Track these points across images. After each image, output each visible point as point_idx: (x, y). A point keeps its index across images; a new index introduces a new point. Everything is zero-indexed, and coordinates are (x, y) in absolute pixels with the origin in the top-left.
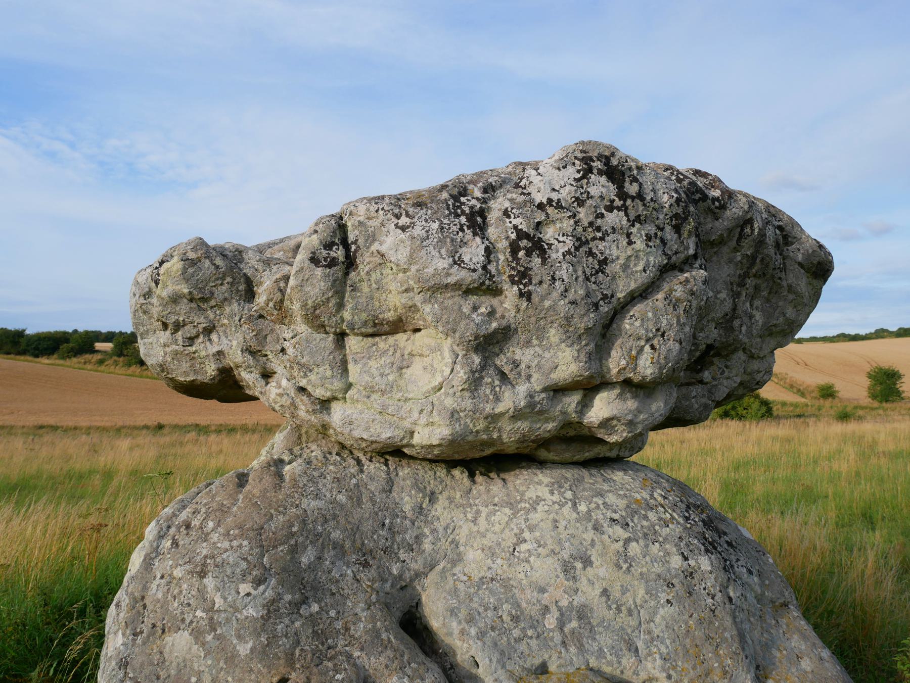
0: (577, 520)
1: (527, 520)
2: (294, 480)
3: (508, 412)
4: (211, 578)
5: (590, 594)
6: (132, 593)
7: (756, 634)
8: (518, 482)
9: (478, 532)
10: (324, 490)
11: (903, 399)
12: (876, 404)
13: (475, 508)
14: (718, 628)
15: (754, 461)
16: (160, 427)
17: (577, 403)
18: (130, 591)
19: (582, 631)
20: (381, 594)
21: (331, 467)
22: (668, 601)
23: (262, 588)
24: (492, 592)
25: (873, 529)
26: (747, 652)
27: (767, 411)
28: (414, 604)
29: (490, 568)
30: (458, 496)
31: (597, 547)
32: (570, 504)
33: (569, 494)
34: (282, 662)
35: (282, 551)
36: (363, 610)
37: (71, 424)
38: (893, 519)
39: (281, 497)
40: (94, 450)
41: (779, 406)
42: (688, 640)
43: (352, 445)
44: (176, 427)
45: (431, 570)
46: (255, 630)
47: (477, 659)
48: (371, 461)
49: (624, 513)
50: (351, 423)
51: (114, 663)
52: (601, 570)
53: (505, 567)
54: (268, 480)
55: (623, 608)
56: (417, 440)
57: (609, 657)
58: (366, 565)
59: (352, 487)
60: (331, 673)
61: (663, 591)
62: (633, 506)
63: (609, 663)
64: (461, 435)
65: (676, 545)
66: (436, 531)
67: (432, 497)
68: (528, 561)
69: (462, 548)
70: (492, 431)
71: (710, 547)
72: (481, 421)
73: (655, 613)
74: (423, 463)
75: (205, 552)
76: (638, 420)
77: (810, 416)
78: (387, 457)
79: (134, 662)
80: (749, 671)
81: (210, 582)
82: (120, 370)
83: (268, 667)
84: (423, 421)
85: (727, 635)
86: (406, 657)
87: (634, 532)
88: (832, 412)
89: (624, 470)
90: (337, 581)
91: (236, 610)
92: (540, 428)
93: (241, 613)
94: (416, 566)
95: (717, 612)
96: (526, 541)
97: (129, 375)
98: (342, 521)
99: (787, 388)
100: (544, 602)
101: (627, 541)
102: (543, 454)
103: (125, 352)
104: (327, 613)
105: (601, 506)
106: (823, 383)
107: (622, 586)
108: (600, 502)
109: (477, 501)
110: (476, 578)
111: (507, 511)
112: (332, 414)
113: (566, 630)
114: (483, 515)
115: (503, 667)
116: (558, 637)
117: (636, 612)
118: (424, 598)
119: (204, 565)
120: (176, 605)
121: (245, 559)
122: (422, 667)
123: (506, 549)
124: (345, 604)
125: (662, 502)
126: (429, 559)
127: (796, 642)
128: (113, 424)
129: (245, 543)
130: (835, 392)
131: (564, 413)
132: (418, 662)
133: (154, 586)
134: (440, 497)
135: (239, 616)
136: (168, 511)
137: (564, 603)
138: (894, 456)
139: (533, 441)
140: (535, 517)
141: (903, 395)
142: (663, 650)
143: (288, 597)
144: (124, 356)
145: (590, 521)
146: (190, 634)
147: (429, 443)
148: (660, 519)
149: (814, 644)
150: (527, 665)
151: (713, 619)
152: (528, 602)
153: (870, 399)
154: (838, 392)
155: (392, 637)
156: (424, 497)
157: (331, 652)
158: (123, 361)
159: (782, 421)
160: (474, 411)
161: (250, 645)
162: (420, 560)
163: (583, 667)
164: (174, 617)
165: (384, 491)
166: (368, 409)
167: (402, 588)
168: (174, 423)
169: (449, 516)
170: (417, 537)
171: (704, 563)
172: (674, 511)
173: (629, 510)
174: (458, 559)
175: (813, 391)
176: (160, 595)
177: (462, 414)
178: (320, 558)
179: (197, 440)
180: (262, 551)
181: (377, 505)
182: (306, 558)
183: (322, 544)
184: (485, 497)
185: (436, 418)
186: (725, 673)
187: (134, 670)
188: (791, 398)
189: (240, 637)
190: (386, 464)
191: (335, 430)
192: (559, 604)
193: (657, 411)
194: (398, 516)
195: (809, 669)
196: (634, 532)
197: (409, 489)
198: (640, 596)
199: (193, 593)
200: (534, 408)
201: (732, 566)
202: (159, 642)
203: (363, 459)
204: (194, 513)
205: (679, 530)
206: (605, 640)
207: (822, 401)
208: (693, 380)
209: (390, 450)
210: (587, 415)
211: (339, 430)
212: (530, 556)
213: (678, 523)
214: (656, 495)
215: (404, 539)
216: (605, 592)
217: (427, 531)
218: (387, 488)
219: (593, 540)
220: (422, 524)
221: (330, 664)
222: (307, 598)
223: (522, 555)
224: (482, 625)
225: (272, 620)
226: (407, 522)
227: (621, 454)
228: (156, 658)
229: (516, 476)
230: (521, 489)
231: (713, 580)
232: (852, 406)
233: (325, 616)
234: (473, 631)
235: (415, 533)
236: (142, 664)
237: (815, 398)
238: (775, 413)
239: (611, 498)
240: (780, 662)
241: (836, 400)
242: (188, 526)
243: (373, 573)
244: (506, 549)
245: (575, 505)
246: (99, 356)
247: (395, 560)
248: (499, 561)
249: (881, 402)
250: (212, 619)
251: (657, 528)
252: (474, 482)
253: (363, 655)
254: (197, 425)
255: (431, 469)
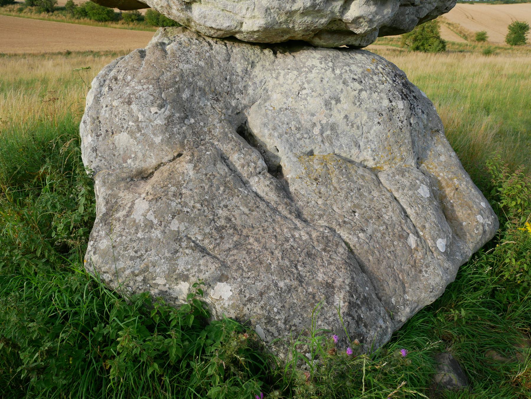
0: (334, 78)
1: (306, 77)
2: (174, 54)
3: (299, 10)
4: (134, 105)
5: (338, 117)
6: (91, 116)
7: (421, 143)
8: (302, 57)
9: (279, 84)
10: (191, 59)
11: (525, 43)
12: (509, 46)
13: (277, 71)
14: (402, 137)
15: (430, 76)
16: (69, 53)
17: (341, 6)
18: (90, 114)
19: (332, 136)
20: (227, 116)
21: (194, 46)
22: (379, 123)
23: (163, 110)
24: (285, 115)
25: (488, 115)
26: (415, 150)
27: (442, 47)
28: (244, 122)
29: (285, 103)
30: (267, 64)
31: (344, 93)
32: (331, 69)
33: (330, 64)
34: (178, 146)
35: (172, 91)
36: (218, 123)
37: (12, 52)
38: (500, 110)
39: (167, 62)
40: (31, 67)
41: (450, 45)
42: (386, 143)
43: (206, 33)
44: (79, 53)
45: (253, 104)
46: (162, 131)
47: (278, 148)
48: (216, 43)
49: (360, 76)
50: (205, 17)
51: (89, 150)
52: (345, 105)
53: (293, 102)
54: (158, 53)
55: (355, 125)
56: (244, 28)
57: (345, 149)
58: (217, 100)
59: (207, 57)
60: (204, 151)
61: (377, 117)
62: (366, 72)
63: (345, 152)
64: (271, 24)
65: (386, 94)
66: (255, 83)
67: (253, 65)
68: (306, 99)
69: (269, 93)
70: (289, 23)
71: (404, 97)
72: (283, 16)
73: (371, 129)
74: (247, 45)
75: (128, 92)
76: (375, 19)
77: (468, 52)
78: (226, 41)
79: (100, 149)
80: (414, 159)
81: (134, 107)
82: (35, 16)
83: (171, 148)
84: (248, 15)
85: (406, 141)
86: (242, 145)
87: (365, 86)
88: (481, 50)
89: (362, 54)
90: (203, 108)
91: (151, 121)
92: (317, 22)
93: (153, 122)
94: (245, 102)
95: (403, 130)
96: (305, 89)
97: (41, 19)
98: (203, 76)
99: (457, 33)
100: (313, 121)
101: (361, 91)
102: (317, 41)
103: (35, 3)
104: (199, 123)
105: (348, 71)
106: (480, 31)
107: (355, 114)
108: (348, 69)
109: (278, 67)
110: (277, 108)
111: (295, 72)
112: (193, 12)
113: (324, 135)
114: (282, 75)
115: (291, 151)
116: (320, 139)
117: (361, 128)
118: (249, 119)
119: (129, 98)
120: (117, 120)
121: (152, 95)
122: (250, 150)
123: (294, 93)
124: (208, 120)
125: (382, 71)
126: (252, 98)
127: (440, 148)
128: (39, 52)
129: (151, 86)
130: (486, 37)
131: (332, 12)
132: (247, 148)
133: (103, 111)
134: (257, 65)
135: (153, 124)
136: (102, 72)
137: (324, 122)
138: (510, 77)
139: (313, 31)
140: (311, 76)
141: (526, 41)
142: (373, 147)
143: (177, 115)
144: (35, 6)
145: (341, 79)
146: (128, 134)
147: (252, 30)
148: (380, 80)
149: (448, 149)
150: (304, 151)
151: (400, 133)
152: (305, 121)
153: (506, 43)
154: (487, 37)
155: (233, 136)
156: (248, 64)
157: (203, 142)
158: (35, 9)
159: (451, 54)
160: (279, 9)
161: (160, 138)
162: (247, 99)
163: (332, 153)
164: (118, 126)
165: (225, 60)
166: (215, 7)
167: (237, 114)
168: (77, 50)
169: (263, 75)
170: (245, 86)
171: (400, 104)
172: (388, 76)
173: (363, 74)
174: (268, 98)
175: (473, 36)
176: (107, 116)
177: (272, 11)
178: (192, 96)
179: (94, 61)
180: (160, 91)
181: (222, 68)
182: (185, 95)
183: (193, 88)
184: (283, 65)
185: (256, 13)
186: (402, 159)
187: (101, 153)
188: (459, 40)
189: (154, 134)
190: (226, 46)
191: (195, 22)
192: (322, 122)
193: (387, 14)
194: (234, 75)
195: (443, 160)
196: (365, 86)
197: (239, 59)
198: (364, 119)
199: (126, 113)
200: (315, 8)
201: (414, 108)
202: (111, 139)
203: (212, 42)
204: (118, 72)
205: (389, 86)
206: (344, 141)
207: (476, 43)
208: (409, 3)
209: (228, 36)
210: (346, 15)
211: (197, 22)
212: (307, 97)
213: (389, 83)
214: (379, 67)
215: (238, 87)
216: (346, 117)
217: (250, 83)
218: (227, 59)
219: (342, 89)
220: (248, 80)
221: (203, 147)
222: (188, 116)
223: (303, 96)
224: (280, 131)
225: (170, 126)
226: (239, 78)
227: (362, 44)
228: (111, 146)
229: (301, 54)
230: (303, 60)
231: (403, 114)
232: (494, 46)
233: (198, 125)
234: (276, 134)
235: (244, 85)
236: (104, 150)
237: (473, 41)
238: (447, 49)
239: (354, 67)
240: (430, 156)
241: (486, 42)
242: (116, 79)
243: (221, 104)
244: (294, 93)
245: (333, 70)
246: (18, 7)
247: (233, 98)
248: (290, 99)
249: (512, 45)
250: (138, 126)
251: (377, 84)
252: (276, 57)
253: (220, 144)
254: (92, 52)
255: (252, 49)
